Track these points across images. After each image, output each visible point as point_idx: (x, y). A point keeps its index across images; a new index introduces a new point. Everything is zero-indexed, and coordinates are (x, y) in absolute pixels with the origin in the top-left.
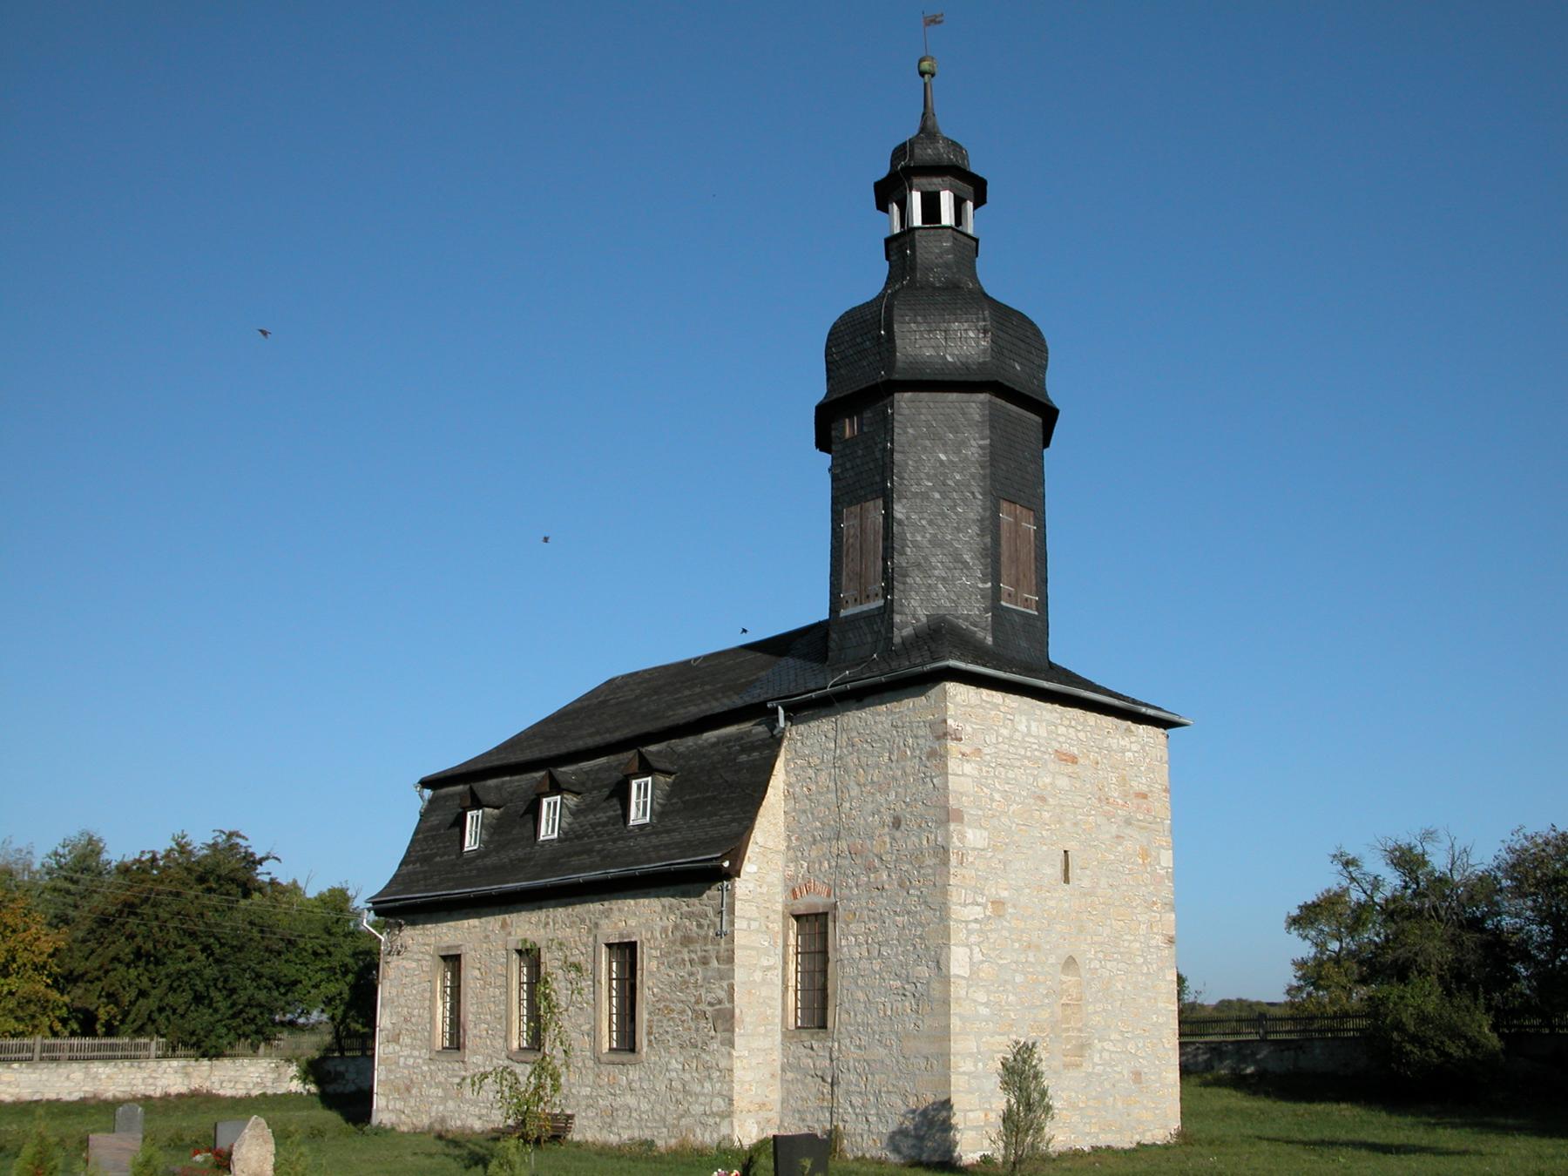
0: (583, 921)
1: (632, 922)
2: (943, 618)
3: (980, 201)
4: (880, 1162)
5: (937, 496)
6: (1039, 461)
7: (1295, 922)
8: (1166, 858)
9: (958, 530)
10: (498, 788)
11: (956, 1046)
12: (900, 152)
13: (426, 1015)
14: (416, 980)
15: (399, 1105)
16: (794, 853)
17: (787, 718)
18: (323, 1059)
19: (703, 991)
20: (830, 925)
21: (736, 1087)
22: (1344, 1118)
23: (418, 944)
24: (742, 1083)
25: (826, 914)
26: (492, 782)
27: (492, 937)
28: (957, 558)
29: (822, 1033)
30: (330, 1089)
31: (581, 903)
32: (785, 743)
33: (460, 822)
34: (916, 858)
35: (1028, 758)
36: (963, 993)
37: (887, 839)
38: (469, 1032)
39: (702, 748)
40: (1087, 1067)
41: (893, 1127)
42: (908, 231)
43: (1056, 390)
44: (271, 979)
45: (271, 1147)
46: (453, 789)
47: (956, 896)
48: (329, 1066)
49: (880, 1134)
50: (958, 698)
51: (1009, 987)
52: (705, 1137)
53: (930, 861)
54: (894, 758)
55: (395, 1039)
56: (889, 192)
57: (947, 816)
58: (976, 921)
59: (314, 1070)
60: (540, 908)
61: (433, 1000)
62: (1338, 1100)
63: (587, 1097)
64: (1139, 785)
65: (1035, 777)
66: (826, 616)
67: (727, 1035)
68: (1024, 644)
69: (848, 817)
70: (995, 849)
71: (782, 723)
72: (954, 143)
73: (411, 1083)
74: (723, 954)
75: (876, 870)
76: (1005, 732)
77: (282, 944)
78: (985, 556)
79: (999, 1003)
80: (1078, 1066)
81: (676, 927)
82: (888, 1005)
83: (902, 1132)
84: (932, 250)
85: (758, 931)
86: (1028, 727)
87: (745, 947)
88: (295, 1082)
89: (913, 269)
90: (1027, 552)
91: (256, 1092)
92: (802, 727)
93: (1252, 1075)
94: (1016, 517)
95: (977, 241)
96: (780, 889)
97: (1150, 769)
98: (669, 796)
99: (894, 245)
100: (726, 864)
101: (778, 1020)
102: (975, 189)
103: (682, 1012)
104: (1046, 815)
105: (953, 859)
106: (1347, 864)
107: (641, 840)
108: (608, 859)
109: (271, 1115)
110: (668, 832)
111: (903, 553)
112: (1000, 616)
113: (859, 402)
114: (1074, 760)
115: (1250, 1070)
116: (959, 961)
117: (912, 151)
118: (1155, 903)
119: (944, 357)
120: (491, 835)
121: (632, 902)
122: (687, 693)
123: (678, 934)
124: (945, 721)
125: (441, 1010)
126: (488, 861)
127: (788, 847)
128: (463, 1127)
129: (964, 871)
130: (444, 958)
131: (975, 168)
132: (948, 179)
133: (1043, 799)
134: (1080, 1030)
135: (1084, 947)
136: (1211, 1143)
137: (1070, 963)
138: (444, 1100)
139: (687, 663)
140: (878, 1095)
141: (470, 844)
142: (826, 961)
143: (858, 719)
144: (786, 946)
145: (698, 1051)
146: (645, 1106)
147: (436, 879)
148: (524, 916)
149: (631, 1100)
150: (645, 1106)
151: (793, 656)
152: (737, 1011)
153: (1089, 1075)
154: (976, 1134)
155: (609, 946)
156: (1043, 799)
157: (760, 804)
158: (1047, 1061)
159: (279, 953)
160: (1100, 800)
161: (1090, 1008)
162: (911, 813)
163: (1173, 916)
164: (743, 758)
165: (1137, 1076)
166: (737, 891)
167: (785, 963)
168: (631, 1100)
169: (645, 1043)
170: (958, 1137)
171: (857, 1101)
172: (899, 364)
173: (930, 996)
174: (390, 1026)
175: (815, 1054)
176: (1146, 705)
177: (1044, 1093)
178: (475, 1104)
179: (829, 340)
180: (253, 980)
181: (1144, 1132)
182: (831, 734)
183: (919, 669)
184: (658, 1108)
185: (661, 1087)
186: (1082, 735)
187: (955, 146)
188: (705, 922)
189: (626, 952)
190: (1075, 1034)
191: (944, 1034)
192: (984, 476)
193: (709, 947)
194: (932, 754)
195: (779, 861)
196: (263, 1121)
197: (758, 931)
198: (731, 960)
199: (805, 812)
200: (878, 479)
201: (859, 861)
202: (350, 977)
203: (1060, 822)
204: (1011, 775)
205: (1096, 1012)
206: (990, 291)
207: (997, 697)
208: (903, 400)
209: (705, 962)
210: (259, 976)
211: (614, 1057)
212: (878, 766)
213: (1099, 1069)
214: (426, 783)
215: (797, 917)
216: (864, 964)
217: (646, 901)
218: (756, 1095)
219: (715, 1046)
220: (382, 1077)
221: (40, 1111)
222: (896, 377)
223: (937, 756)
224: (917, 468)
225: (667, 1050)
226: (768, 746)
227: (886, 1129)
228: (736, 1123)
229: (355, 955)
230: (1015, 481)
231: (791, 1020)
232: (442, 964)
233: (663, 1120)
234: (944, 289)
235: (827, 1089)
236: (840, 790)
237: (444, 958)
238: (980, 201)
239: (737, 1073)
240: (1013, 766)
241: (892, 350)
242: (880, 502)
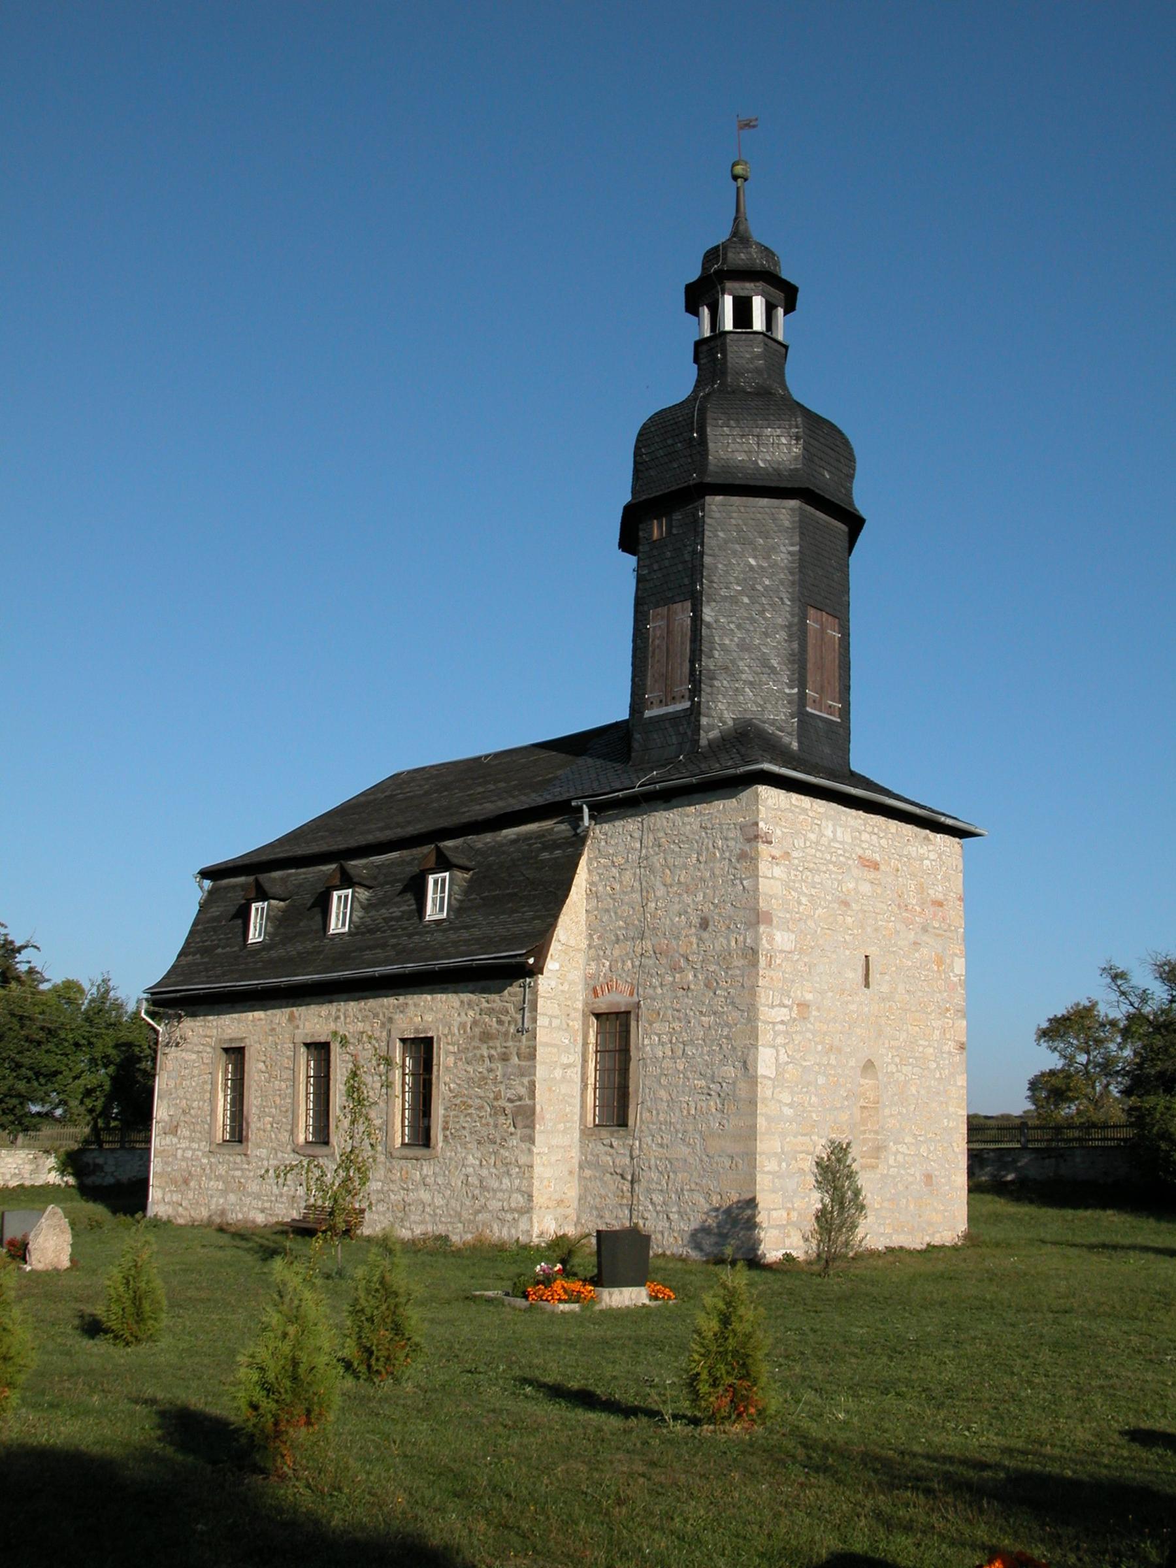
0: (376, 1016)
1: (429, 1018)
2: (749, 723)
3: (790, 308)
4: (683, 1260)
5: (746, 600)
6: (844, 569)
7: (1044, 1034)
8: (959, 966)
9: (766, 634)
10: (283, 880)
11: (761, 1146)
12: (712, 255)
13: (207, 1106)
14: (196, 1072)
15: (176, 1197)
16: (596, 952)
17: (591, 817)
18: (81, 1151)
19: (502, 1088)
20: (633, 1024)
21: (536, 1183)
22: (1113, 1223)
23: (199, 1036)
24: (541, 1180)
25: (629, 1012)
26: (276, 874)
27: (278, 1029)
28: (765, 663)
29: (622, 1131)
30: (89, 1181)
31: (374, 997)
32: (589, 842)
33: (243, 914)
34: (724, 958)
35: (831, 862)
36: (769, 1093)
37: (694, 940)
38: (252, 1126)
39: (501, 845)
40: (882, 1169)
41: (695, 1225)
42: (718, 335)
43: (862, 501)
44: (31, 1069)
45: (68, 1237)
46: (233, 882)
47: (764, 997)
48: (88, 1158)
49: (681, 1231)
50: (770, 802)
52: (500, 1233)
53: (738, 962)
54: (703, 859)
55: (173, 1130)
56: (700, 295)
57: (756, 918)
58: (782, 1022)
59: (72, 1162)
60: (331, 1002)
61: (213, 1092)
62: (1104, 1207)
63: (378, 1191)
64: (936, 893)
65: (840, 882)
66: (624, 715)
67: (528, 1131)
68: (827, 750)
69: (653, 916)
70: (801, 952)
71: (586, 822)
72: (766, 248)
73: (192, 1171)
74: (524, 1050)
75: (682, 970)
76: (813, 837)
77: (42, 1034)
78: (792, 662)
79: (801, 1104)
80: (874, 1167)
81: (475, 1023)
82: (692, 1104)
83: (704, 1230)
84: (743, 356)
85: (559, 1028)
86: (834, 832)
87: (547, 1045)
88: (53, 1173)
89: (724, 373)
90: (832, 659)
91: (13, 1183)
92: (606, 826)
93: (1012, 1182)
94: (822, 625)
95: (786, 347)
96: (580, 987)
97: (946, 878)
98: (467, 892)
99: (705, 348)
100: (531, 961)
101: (577, 1118)
102: (786, 296)
103: (481, 1108)
104: (849, 920)
105: (762, 961)
106: (1115, 977)
107: (439, 936)
108: (404, 954)
109: (69, 1205)
110: (467, 928)
111: (711, 656)
112: (805, 721)
113: (667, 506)
114: (876, 866)
115: (1010, 1177)
116: (766, 1062)
117: (725, 254)
119: (756, 462)
120: (277, 928)
121: (429, 997)
122: (480, 789)
123: (477, 1030)
124: (757, 824)
125: (222, 1103)
126: (274, 954)
127: (590, 946)
128: (246, 1221)
130: (226, 1050)
131: (786, 274)
132: (760, 285)
133: (846, 904)
134: (876, 1132)
135: (883, 1051)
136: (997, 1245)
137: (869, 1066)
138: (224, 1193)
139: (477, 760)
140: (680, 1193)
141: (255, 936)
142: (243, 1085)
143: (664, 819)
144: (585, 1044)
145: (496, 1147)
146: (439, 1201)
147: (219, 971)
148: (314, 1009)
149: (425, 1196)
150: (439, 1201)
151: (591, 756)
152: (538, 1108)
153: (884, 1176)
154: (784, 1233)
155: (403, 1040)
157: (563, 902)
158: (857, 1158)
159: (39, 1043)
160: (899, 906)
161: (887, 1111)
162: (720, 914)
163: (965, 1023)
164: (545, 855)
165: (928, 1178)
166: (540, 987)
167: (585, 1060)
168: (425, 1196)
169: (440, 1138)
170: (762, 1235)
171: (658, 1198)
172: (711, 468)
173: (737, 1096)
174: (167, 1118)
175: (615, 1150)
176: (943, 815)
177: (857, 1193)
178: (258, 1197)
179: (638, 441)
180: (13, 1070)
181: (933, 1234)
182: (637, 834)
183: (732, 771)
184: (453, 1202)
185: (457, 1182)
186: (883, 842)
187: (767, 252)
188: (506, 1019)
189: (422, 1049)
190: (872, 1136)
191: (750, 1134)
192: (793, 583)
193: (510, 1044)
194: (743, 856)
195: (581, 959)
196: (60, 1210)
197: (559, 1028)
198: (532, 1056)
199: (607, 911)
200: (686, 581)
201: (664, 961)
202: (111, 1069)
203: (862, 927)
204: (817, 879)
205: (891, 1115)
206: (797, 396)
207: (805, 801)
208: (715, 503)
209: (505, 1058)
210: (19, 1066)
211: (407, 1152)
212: (685, 867)
213: (893, 1171)
214: (205, 874)
215: (598, 1016)
216: (667, 1063)
217: (444, 996)
218: (554, 1189)
219: (514, 1142)
220: (158, 1169)
222: (708, 480)
223: (748, 858)
224: (727, 572)
225: (464, 1145)
226: (572, 844)
227: (688, 1227)
228: (535, 1220)
229: (116, 1046)
230: (822, 589)
231: (590, 1117)
232: (224, 1056)
233: (459, 1215)
234: (758, 394)
235: (626, 1186)
236: (646, 891)
237: (226, 1050)
238: (790, 308)
239: (537, 1170)
240: (818, 870)
241: (704, 452)
242: (688, 604)
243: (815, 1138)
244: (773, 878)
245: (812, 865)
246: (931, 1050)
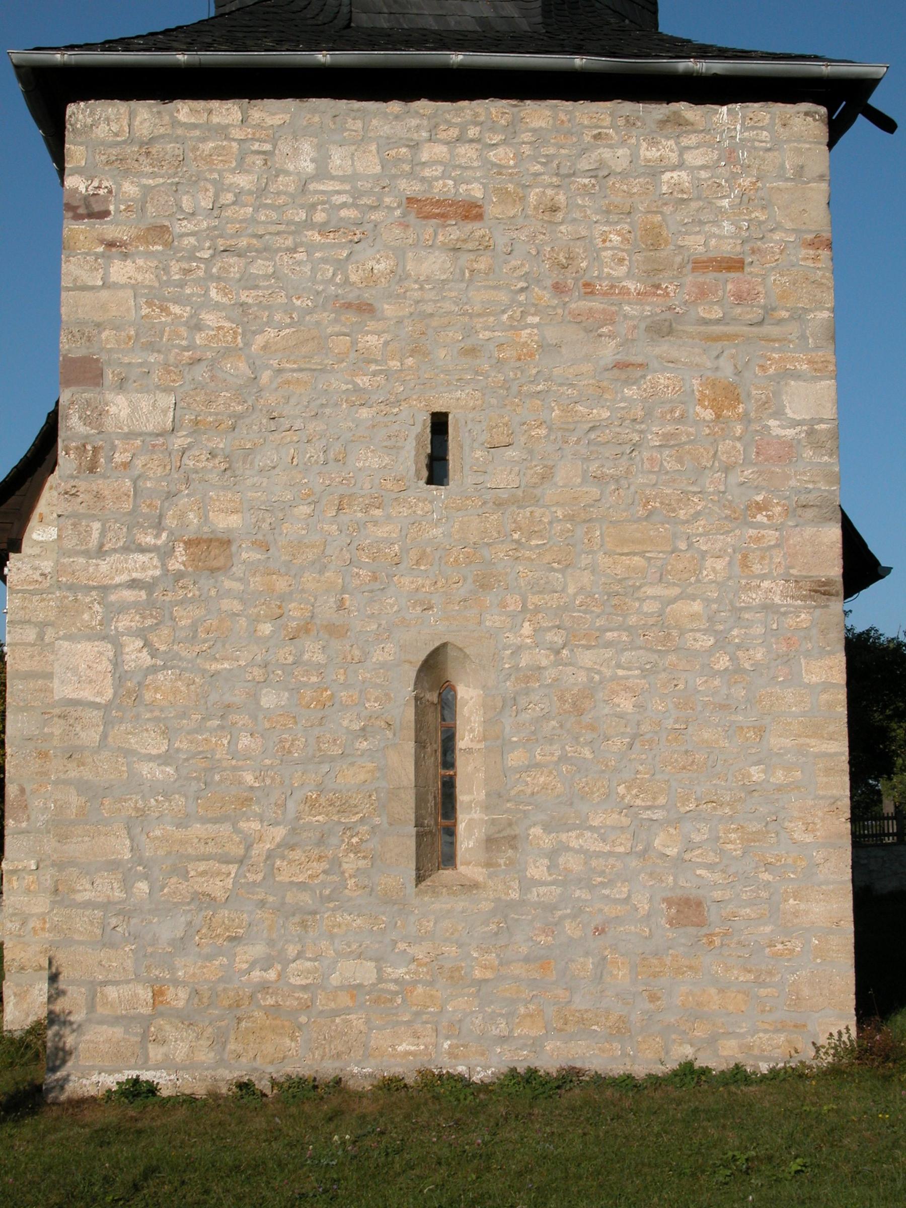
8: (810, 400)
50: (102, 131)
51: (241, 719)
114: (471, 211)
129: (99, 484)
186: (498, 155)
221: (447, 823)
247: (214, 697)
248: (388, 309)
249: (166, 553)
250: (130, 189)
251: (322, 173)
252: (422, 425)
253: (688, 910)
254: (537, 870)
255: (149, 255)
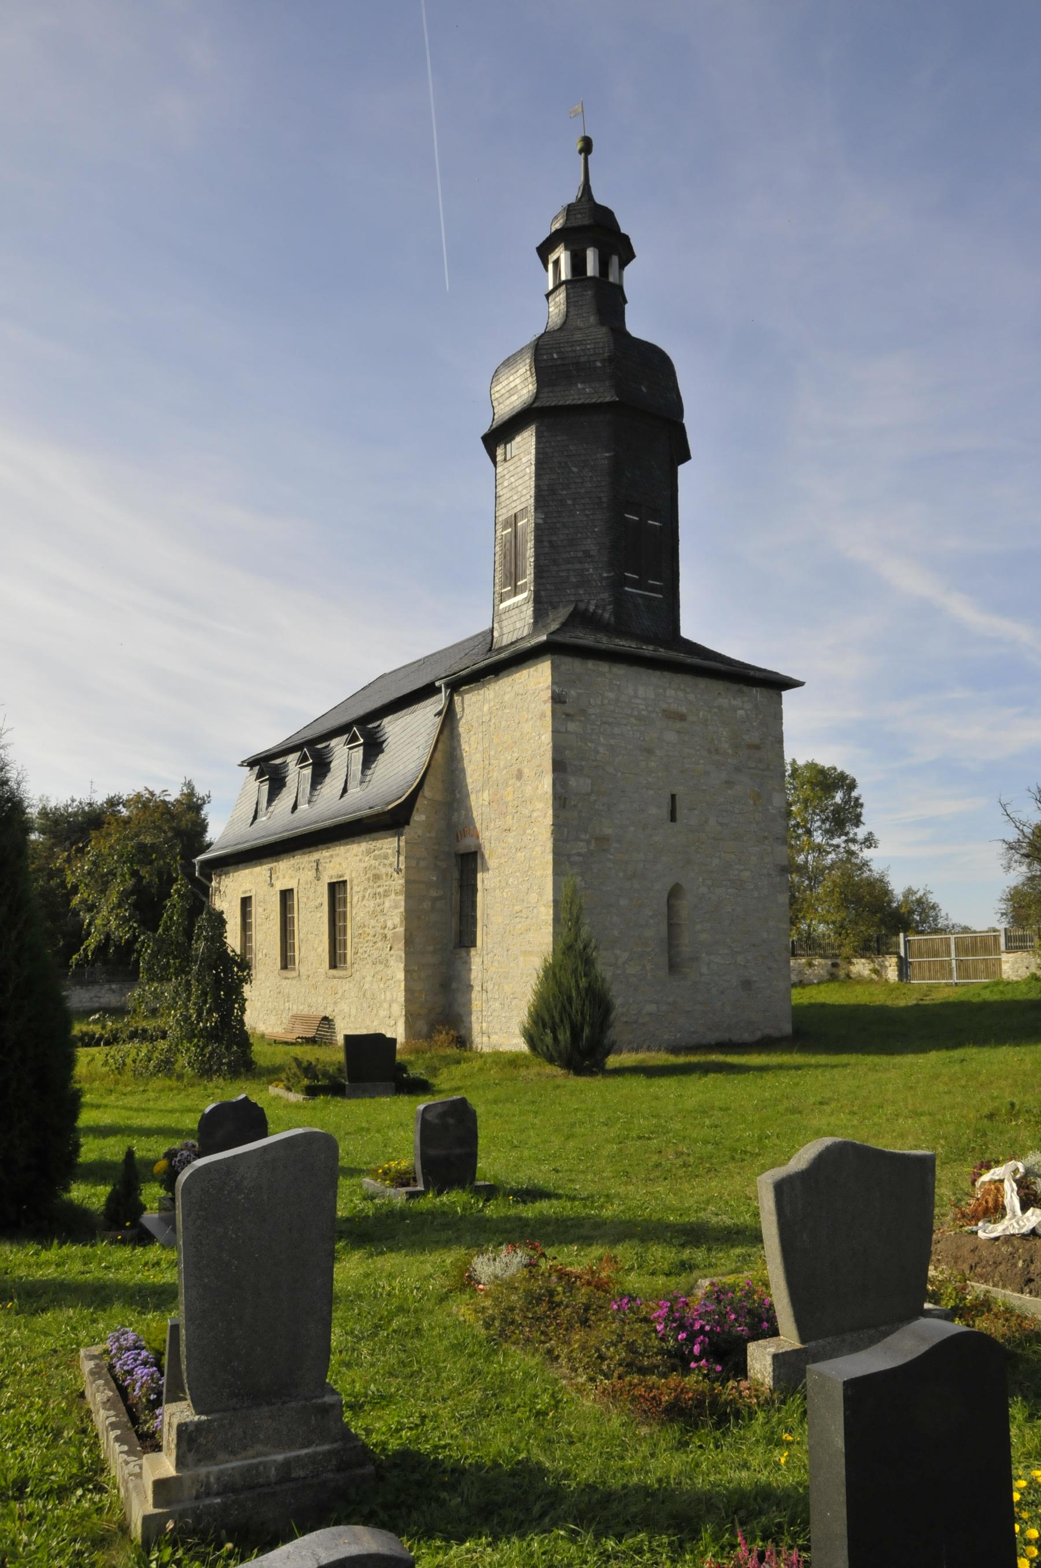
114: (682, 718)
118: (766, 838)
156: (650, 751)
204: (616, 731)
243: (618, 952)
244: (567, 732)
245: (610, 720)
246: (748, 874)
247: (544, 1265)
248: (658, 752)
249: (588, 842)
250: (573, 693)
251: (636, 697)
252: (668, 799)
253: (747, 984)
254: (704, 970)
255: (580, 721)
